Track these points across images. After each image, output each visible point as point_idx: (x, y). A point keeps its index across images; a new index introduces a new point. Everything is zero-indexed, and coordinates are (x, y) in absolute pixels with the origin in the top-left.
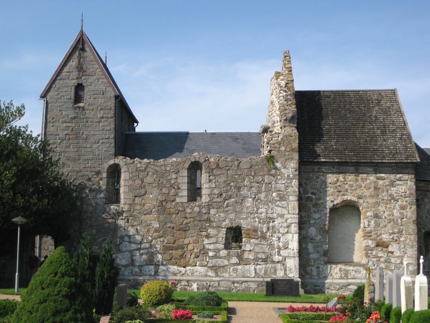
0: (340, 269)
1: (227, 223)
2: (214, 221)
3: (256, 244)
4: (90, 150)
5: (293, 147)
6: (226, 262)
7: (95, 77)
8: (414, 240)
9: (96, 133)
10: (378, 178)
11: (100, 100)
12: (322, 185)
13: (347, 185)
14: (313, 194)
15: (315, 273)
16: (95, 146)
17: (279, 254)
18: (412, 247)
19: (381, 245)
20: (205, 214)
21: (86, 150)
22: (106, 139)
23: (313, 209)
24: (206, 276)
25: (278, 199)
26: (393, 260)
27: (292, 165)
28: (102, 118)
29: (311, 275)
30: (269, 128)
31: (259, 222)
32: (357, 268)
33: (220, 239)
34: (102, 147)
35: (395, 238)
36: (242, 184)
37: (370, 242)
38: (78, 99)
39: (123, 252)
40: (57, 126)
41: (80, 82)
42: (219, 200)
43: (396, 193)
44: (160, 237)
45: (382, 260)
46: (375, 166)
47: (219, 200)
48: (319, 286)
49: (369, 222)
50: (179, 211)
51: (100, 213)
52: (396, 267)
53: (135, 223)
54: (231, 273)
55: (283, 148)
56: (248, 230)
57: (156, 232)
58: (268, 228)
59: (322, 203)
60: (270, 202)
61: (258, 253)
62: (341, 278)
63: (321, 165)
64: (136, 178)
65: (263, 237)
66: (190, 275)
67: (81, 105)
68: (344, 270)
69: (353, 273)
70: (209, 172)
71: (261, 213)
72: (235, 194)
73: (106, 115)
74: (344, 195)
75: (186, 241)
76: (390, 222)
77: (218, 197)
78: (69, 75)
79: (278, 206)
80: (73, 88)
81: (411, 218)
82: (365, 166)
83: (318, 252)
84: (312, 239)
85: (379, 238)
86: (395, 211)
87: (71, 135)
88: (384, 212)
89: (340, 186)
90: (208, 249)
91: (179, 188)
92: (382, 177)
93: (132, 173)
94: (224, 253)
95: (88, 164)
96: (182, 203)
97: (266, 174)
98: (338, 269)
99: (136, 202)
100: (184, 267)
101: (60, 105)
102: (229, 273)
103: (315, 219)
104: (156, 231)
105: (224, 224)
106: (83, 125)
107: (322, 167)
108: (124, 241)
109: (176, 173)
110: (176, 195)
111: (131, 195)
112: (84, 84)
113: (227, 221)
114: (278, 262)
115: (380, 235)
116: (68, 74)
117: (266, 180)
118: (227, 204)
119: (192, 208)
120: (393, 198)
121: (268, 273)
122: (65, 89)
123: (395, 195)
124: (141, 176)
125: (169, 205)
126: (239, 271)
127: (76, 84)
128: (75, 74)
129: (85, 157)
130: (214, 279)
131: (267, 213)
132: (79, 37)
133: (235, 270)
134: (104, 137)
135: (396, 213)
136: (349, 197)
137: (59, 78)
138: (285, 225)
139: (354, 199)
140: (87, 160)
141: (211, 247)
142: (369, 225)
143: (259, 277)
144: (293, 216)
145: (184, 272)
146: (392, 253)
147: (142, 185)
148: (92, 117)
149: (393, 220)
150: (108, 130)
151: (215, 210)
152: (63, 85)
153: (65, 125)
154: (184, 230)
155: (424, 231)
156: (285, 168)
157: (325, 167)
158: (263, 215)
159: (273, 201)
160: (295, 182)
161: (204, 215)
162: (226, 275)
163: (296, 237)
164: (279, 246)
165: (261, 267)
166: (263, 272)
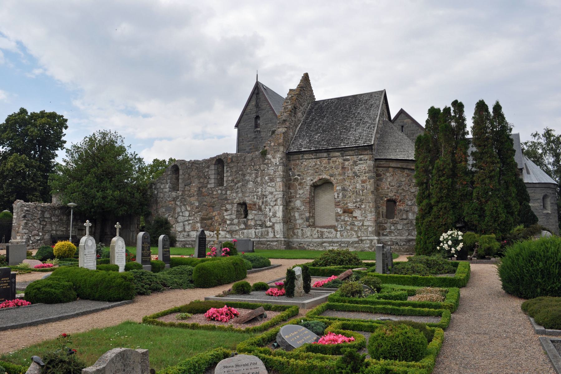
0: (318, 230)
3: (255, 215)
6: (237, 228)
8: (373, 207)
10: (344, 160)
12: (305, 169)
13: (322, 167)
14: (299, 175)
15: (300, 234)
17: (270, 221)
18: (371, 212)
19: (347, 211)
23: (298, 187)
24: (226, 237)
25: (269, 181)
26: (356, 223)
27: (278, 155)
29: (297, 235)
31: (257, 198)
32: (330, 230)
33: (233, 212)
35: (358, 206)
37: (339, 210)
38: (257, 126)
39: (178, 223)
42: (232, 184)
43: (358, 171)
44: (199, 212)
45: (349, 223)
46: (341, 151)
47: (232, 184)
49: (338, 194)
52: (359, 228)
53: (185, 203)
55: (272, 144)
56: (250, 204)
58: (263, 203)
59: (305, 182)
61: (257, 220)
62: (318, 238)
63: (304, 154)
65: (260, 209)
67: (259, 129)
68: (321, 231)
69: (327, 234)
71: (258, 192)
74: (320, 175)
75: (214, 214)
76: (353, 194)
77: (231, 182)
79: (269, 186)
82: (334, 151)
83: (302, 219)
84: (298, 209)
85: (345, 206)
86: (358, 185)
88: (349, 186)
89: (317, 168)
90: (227, 219)
91: (209, 178)
92: (347, 159)
93: (184, 170)
94: (236, 221)
96: (211, 188)
98: (316, 231)
99: (186, 189)
100: (213, 232)
103: (300, 194)
104: (197, 208)
105: (235, 201)
107: (304, 155)
110: (208, 183)
111: (183, 185)
113: (237, 199)
114: (270, 227)
115: (347, 203)
118: (237, 187)
119: (217, 191)
120: (356, 175)
121: (263, 235)
124: (189, 172)
125: (204, 190)
126: (245, 233)
131: (262, 192)
133: (243, 233)
135: (359, 186)
136: (325, 176)
137: (245, 114)
138: (274, 199)
139: (328, 177)
142: (338, 197)
143: (257, 238)
144: (279, 193)
145: (212, 235)
146: (356, 217)
149: (356, 191)
153: (250, 143)
154: (212, 206)
155: (386, 199)
156: (274, 158)
160: (281, 168)
163: (281, 207)
165: (259, 230)
166: (260, 234)
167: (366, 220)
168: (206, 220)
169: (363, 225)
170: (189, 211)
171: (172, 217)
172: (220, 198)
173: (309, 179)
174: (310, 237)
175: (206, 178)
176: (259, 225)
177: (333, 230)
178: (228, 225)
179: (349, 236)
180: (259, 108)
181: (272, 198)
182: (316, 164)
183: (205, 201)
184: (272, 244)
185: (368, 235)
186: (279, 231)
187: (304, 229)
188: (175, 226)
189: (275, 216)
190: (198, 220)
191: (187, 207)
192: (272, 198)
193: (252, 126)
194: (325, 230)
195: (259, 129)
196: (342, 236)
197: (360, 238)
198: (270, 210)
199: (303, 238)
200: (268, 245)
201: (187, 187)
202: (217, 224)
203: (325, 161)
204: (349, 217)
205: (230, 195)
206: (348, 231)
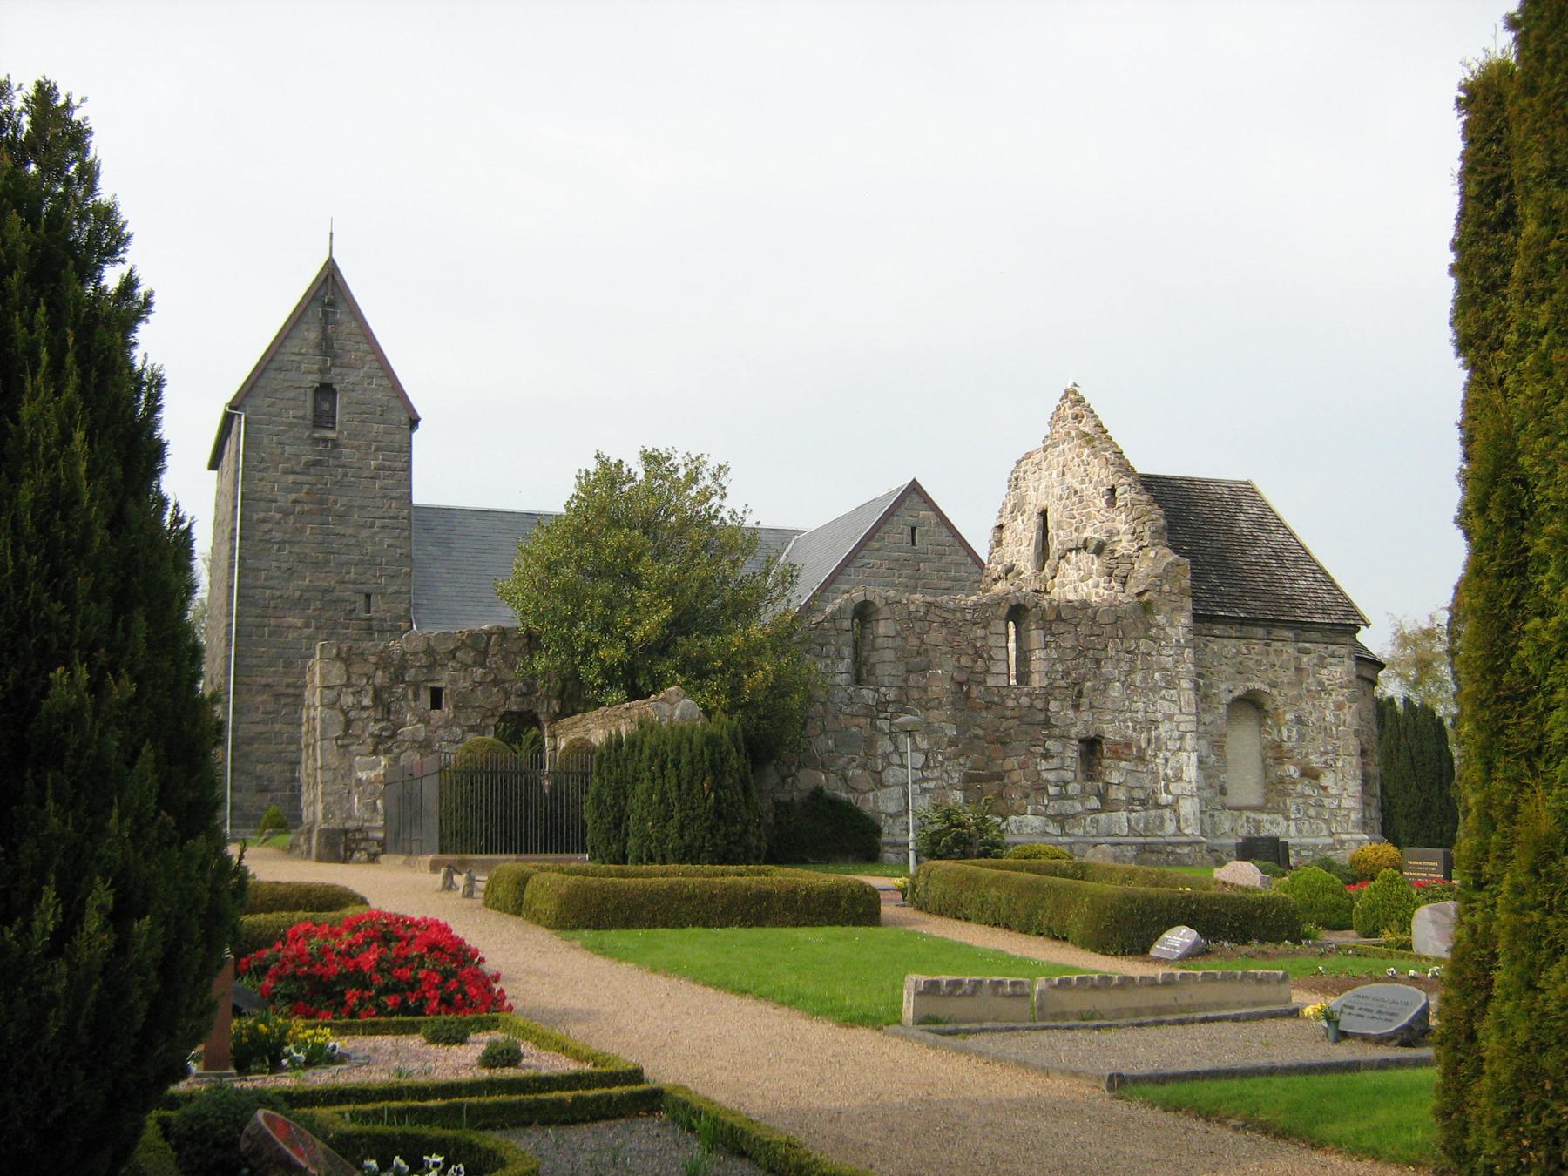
0: (1248, 818)
1: (1078, 730)
2: (1056, 726)
3: (1129, 772)
4: (353, 541)
5: (1183, 585)
6: (1079, 807)
7: (361, 373)
9: (367, 502)
10: (1300, 651)
11: (375, 426)
16: (365, 533)
17: (1167, 791)
18: (1354, 778)
20: (1041, 710)
21: (345, 541)
22: (391, 518)
24: (1045, 833)
26: (1326, 802)
28: (380, 470)
30: (1106, 544)
31: (1134, 729)
34: (380, 536)
36: (1102, 654)
38: (322, 419)
39: (886, 787)
40: (272, 479)
41: (327, 380)
43: (1328, 679)
46: (1297, 628)
47: (1063, 683)
48: (1216, 851)
49: (1289, 731)
50: (993, 703)
51: (841, 705)
52: (1332, 814)
54: (1088, 829)
56: (1116, 743)
57: (950, 746)
58: (1149, 741)
59: (1215, 694)
60: (1150, 690)
61: (1133, 788)
64: (907, 632)
65: (1141, 758)
66: (1015, 832)
68: (1254, 820)
70: (1043, 628)
71: (1136, 712)
72: (1091, 674)
73: (390, 463)
74: (1248, 680)
78: (300, 362)
79: (1163, 698)
80: (310, 393)
81: (1351, 724)
83: (1212, 787)
86: (1327, 712)
87: (306, 503)
89: (1241, 663)
90: (1047, 781)
91: (991, 658)
92: (1306, 649)
95: (349, 573)
97: (1142, 635)
98: (1244, 818)
101: (279, 431)
102: (1085, 827)
105: (1073, 732)
106: (337, 482)
108: (890, 764)
109: (983, 627)
111: (902, 668)
112: (337, 387)
114: (1166, 806)
115: (1307, 754)
116: (298, 358)
117: (1142, 648)
119: (1017, 699)
121: (1151, 826)
122: (291, 394)
123: (1327, 682)
126: (1102, 823)
127: (317, 385)
128: (313, 363)
129: (343, 558)
130: (1060, 839)
131: (1146, 712)
132: (325, 274)
133: (1096, 822)
134: (386, 515)
137: (274, 365)
138: (1176, 734)
139: (1265, 688)
140: (348, 564)
141: (1051, 776)
142: (1289, 737)
143: (1135, 836)
147: (922, 650)
148: (357, 465)
150: (395, 498)
151: (1058, 703)
152: (286, 384)
153: (291, 478)
154: (1003, 741)
156: (1171, 625)
157: (1219, 627)
158: (1140, 715)
159: (1155, 689)
161: (1038, 713)
162: (1079, 831)
164: (1166, 774)
167: (1345, 796)
168: (980, 782)
169: (1339, 807)
170: (926, 753)
171: (863, 766)
172: (1027, 719)
173: (1223, 686)
174: (1231, 833)
175: (981, 657)
176: (1139, 800)
177: (1280, 818)
178: (1052, 798)
179: (1313, 832)
180: (335, 356)
181: (1172, 730)
182: (1239, 652)
183: (980, 726)
184: (1178, 850)
185: (1350, 830)
186: (1191, 817)
187: (1216, 813)
188: (876, 797)
189: (1179, 779)
190: (956, 780)
191: (918, 738)
192: (1172, 730)
193: (303, 418)
194: (1264, 817)
195: (331, 435)
196: (1299, 831)
197: (1336, 837)
198: (1166, 761)
199: (1216, 836)
200: (1169, 854)
201: (913, 677)
202: (1016, 795)
203: (1258, 647)
204: (1313, 787)
205: (1058, 713)
206: (1312, 821)
